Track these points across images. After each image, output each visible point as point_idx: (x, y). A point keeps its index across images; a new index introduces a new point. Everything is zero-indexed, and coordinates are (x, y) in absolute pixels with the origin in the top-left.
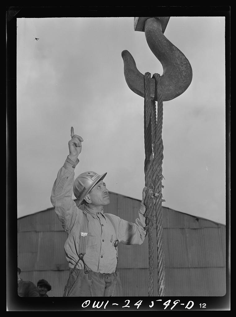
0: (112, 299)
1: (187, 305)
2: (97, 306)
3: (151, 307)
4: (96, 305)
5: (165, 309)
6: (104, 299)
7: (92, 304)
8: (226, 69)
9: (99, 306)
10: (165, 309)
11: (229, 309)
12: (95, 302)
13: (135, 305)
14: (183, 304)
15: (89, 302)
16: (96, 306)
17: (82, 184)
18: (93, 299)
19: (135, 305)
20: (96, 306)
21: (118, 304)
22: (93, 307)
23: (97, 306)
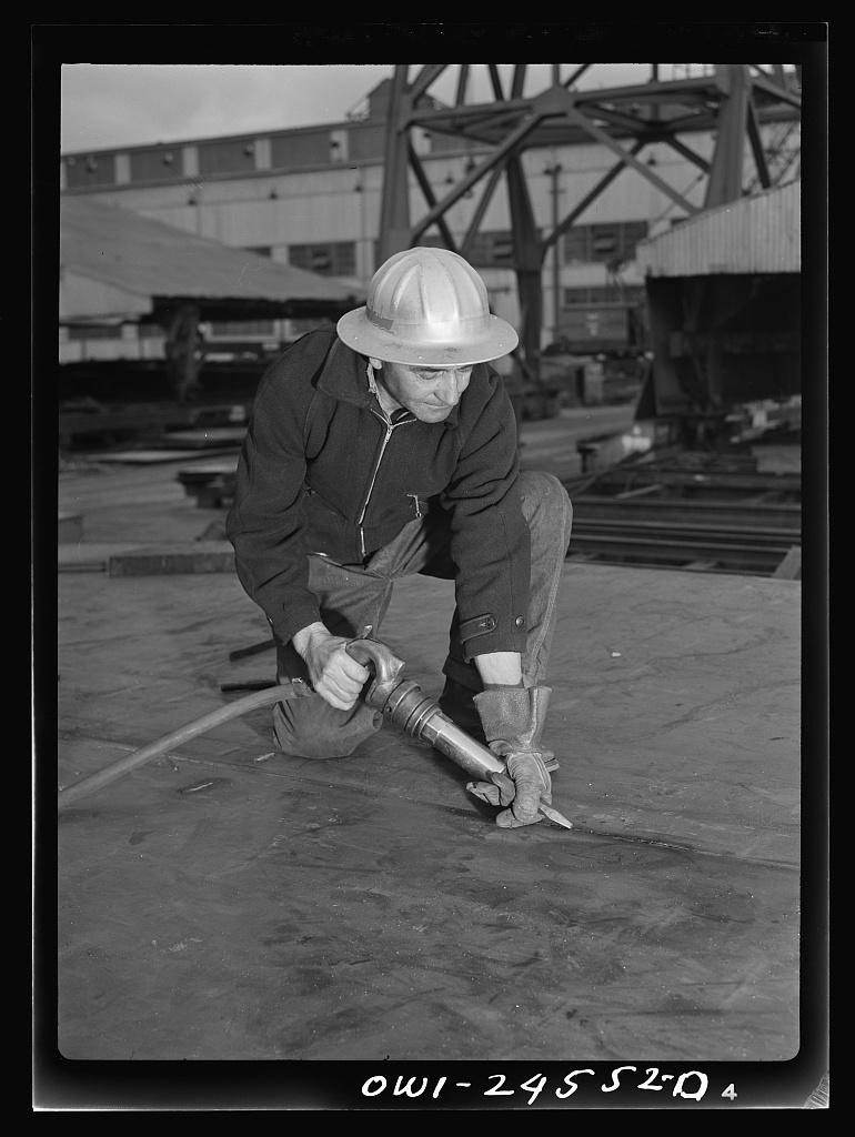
0: (454, 1070)
1: (528, 1082)
2: (408, 1089)
3: (604, 1089)
4: (403, 1085)
5: (530, 1102)
6: (431, 1070)
7: (391, 1086)
8: (264, 64)
9: (414, 1091)
10: (530, 1102)
11: (827, 1107)
12: (401, 1078)
13: (640, 1087)
14: (671, 1077)
15: (380, 1083)
16: (405, 1089)
17: (398, 637)
18: (392, 1069)
19: (640, 1087)
20: (405, 1089)
21: (468, 1085)
22: (397, 1092)
23: (408, 1089)
